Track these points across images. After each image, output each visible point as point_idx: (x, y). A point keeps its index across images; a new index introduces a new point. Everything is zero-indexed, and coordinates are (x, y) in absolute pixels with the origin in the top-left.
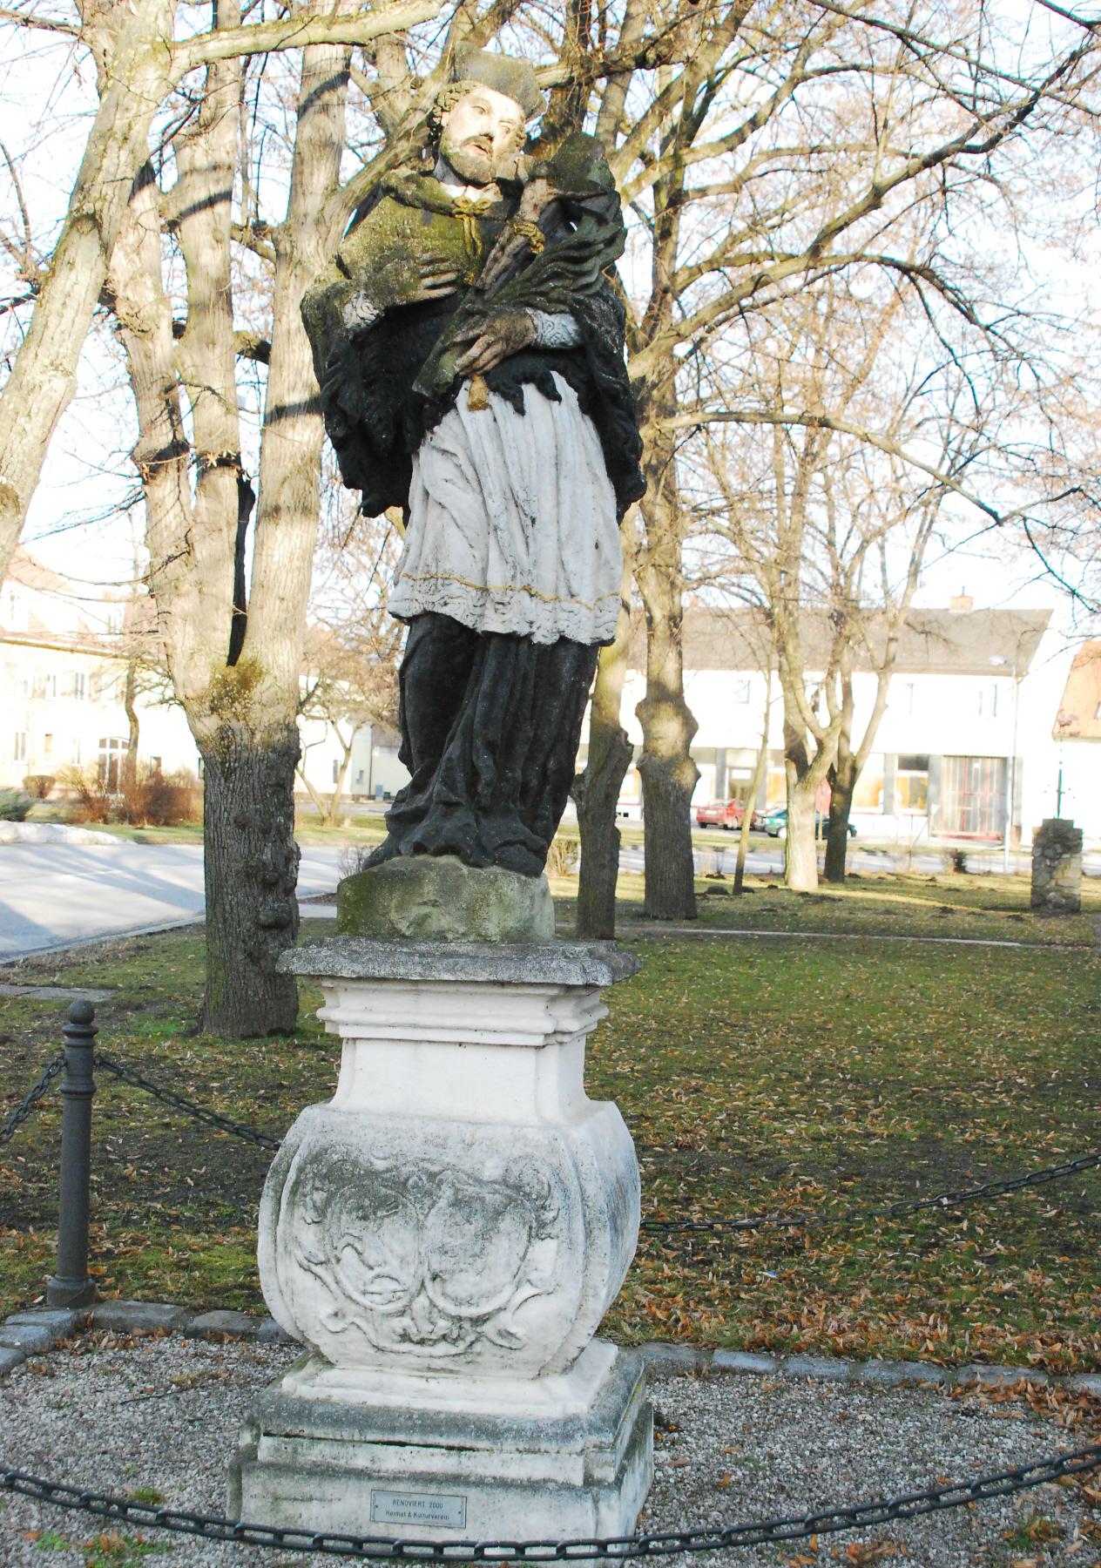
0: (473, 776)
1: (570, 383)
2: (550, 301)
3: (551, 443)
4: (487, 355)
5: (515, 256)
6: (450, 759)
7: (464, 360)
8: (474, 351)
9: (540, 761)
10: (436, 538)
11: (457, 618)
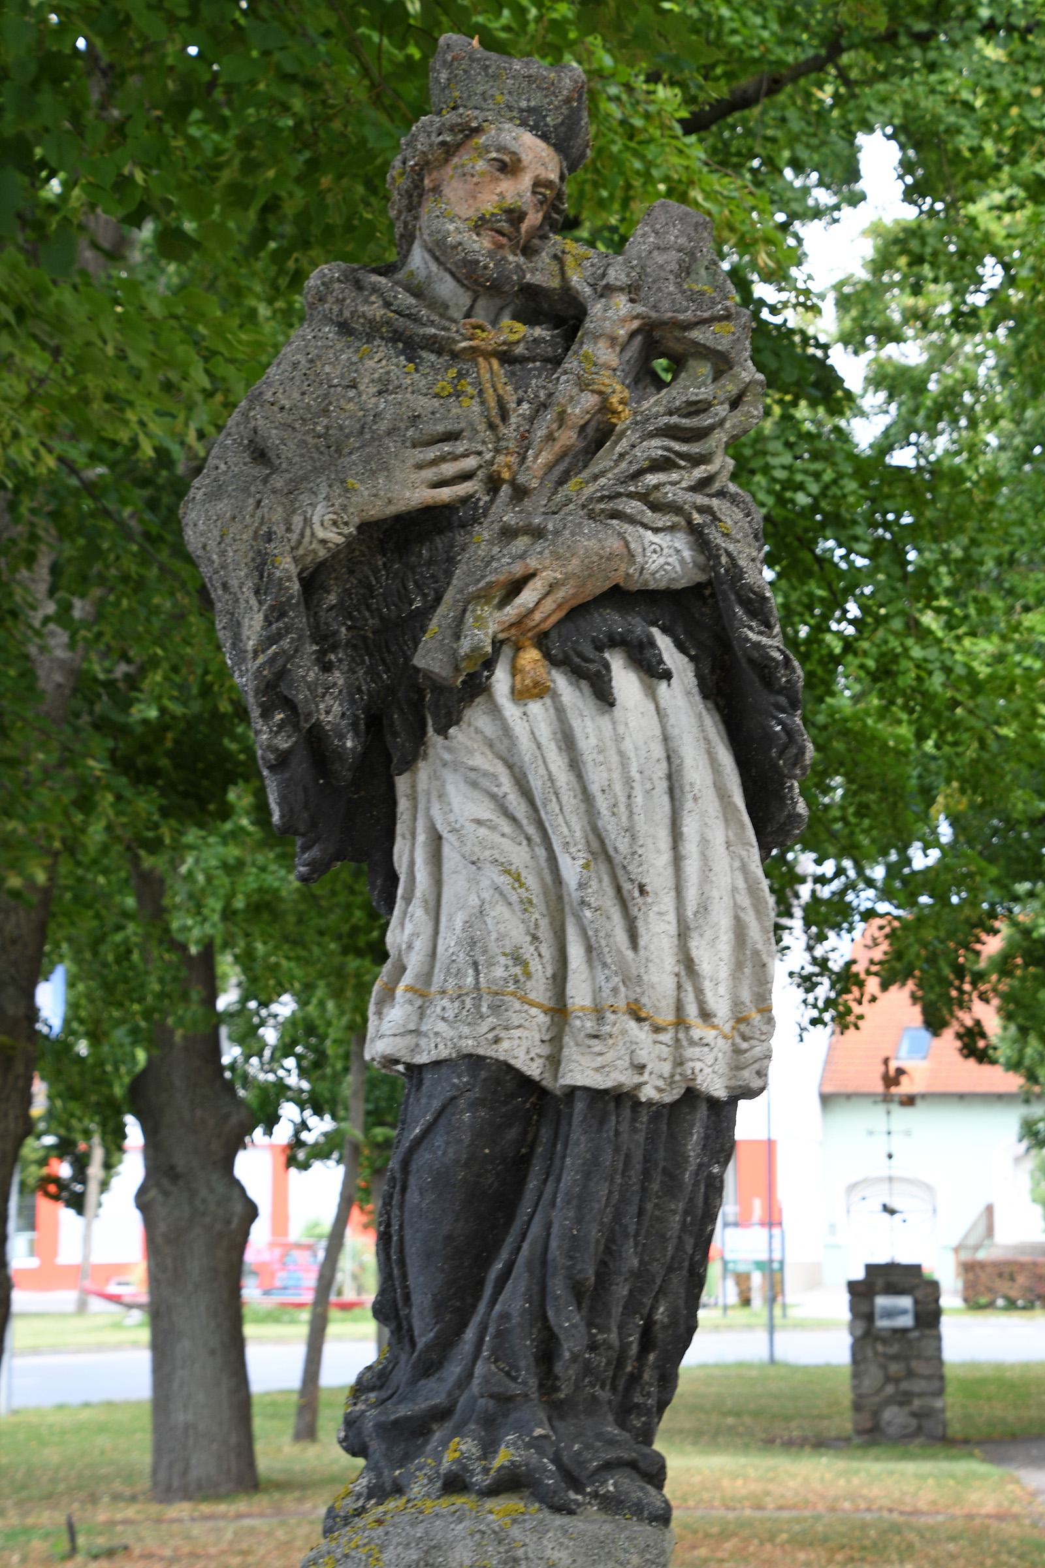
0: (547, 1353)
1: (681, 647)
2: (655, 507)
3: (658, 751)
4: (549, 605)
5: (583, 428)
6: (505, 1316)
7: (512, 611)
8: (528, 597)
9: (646, 1311)
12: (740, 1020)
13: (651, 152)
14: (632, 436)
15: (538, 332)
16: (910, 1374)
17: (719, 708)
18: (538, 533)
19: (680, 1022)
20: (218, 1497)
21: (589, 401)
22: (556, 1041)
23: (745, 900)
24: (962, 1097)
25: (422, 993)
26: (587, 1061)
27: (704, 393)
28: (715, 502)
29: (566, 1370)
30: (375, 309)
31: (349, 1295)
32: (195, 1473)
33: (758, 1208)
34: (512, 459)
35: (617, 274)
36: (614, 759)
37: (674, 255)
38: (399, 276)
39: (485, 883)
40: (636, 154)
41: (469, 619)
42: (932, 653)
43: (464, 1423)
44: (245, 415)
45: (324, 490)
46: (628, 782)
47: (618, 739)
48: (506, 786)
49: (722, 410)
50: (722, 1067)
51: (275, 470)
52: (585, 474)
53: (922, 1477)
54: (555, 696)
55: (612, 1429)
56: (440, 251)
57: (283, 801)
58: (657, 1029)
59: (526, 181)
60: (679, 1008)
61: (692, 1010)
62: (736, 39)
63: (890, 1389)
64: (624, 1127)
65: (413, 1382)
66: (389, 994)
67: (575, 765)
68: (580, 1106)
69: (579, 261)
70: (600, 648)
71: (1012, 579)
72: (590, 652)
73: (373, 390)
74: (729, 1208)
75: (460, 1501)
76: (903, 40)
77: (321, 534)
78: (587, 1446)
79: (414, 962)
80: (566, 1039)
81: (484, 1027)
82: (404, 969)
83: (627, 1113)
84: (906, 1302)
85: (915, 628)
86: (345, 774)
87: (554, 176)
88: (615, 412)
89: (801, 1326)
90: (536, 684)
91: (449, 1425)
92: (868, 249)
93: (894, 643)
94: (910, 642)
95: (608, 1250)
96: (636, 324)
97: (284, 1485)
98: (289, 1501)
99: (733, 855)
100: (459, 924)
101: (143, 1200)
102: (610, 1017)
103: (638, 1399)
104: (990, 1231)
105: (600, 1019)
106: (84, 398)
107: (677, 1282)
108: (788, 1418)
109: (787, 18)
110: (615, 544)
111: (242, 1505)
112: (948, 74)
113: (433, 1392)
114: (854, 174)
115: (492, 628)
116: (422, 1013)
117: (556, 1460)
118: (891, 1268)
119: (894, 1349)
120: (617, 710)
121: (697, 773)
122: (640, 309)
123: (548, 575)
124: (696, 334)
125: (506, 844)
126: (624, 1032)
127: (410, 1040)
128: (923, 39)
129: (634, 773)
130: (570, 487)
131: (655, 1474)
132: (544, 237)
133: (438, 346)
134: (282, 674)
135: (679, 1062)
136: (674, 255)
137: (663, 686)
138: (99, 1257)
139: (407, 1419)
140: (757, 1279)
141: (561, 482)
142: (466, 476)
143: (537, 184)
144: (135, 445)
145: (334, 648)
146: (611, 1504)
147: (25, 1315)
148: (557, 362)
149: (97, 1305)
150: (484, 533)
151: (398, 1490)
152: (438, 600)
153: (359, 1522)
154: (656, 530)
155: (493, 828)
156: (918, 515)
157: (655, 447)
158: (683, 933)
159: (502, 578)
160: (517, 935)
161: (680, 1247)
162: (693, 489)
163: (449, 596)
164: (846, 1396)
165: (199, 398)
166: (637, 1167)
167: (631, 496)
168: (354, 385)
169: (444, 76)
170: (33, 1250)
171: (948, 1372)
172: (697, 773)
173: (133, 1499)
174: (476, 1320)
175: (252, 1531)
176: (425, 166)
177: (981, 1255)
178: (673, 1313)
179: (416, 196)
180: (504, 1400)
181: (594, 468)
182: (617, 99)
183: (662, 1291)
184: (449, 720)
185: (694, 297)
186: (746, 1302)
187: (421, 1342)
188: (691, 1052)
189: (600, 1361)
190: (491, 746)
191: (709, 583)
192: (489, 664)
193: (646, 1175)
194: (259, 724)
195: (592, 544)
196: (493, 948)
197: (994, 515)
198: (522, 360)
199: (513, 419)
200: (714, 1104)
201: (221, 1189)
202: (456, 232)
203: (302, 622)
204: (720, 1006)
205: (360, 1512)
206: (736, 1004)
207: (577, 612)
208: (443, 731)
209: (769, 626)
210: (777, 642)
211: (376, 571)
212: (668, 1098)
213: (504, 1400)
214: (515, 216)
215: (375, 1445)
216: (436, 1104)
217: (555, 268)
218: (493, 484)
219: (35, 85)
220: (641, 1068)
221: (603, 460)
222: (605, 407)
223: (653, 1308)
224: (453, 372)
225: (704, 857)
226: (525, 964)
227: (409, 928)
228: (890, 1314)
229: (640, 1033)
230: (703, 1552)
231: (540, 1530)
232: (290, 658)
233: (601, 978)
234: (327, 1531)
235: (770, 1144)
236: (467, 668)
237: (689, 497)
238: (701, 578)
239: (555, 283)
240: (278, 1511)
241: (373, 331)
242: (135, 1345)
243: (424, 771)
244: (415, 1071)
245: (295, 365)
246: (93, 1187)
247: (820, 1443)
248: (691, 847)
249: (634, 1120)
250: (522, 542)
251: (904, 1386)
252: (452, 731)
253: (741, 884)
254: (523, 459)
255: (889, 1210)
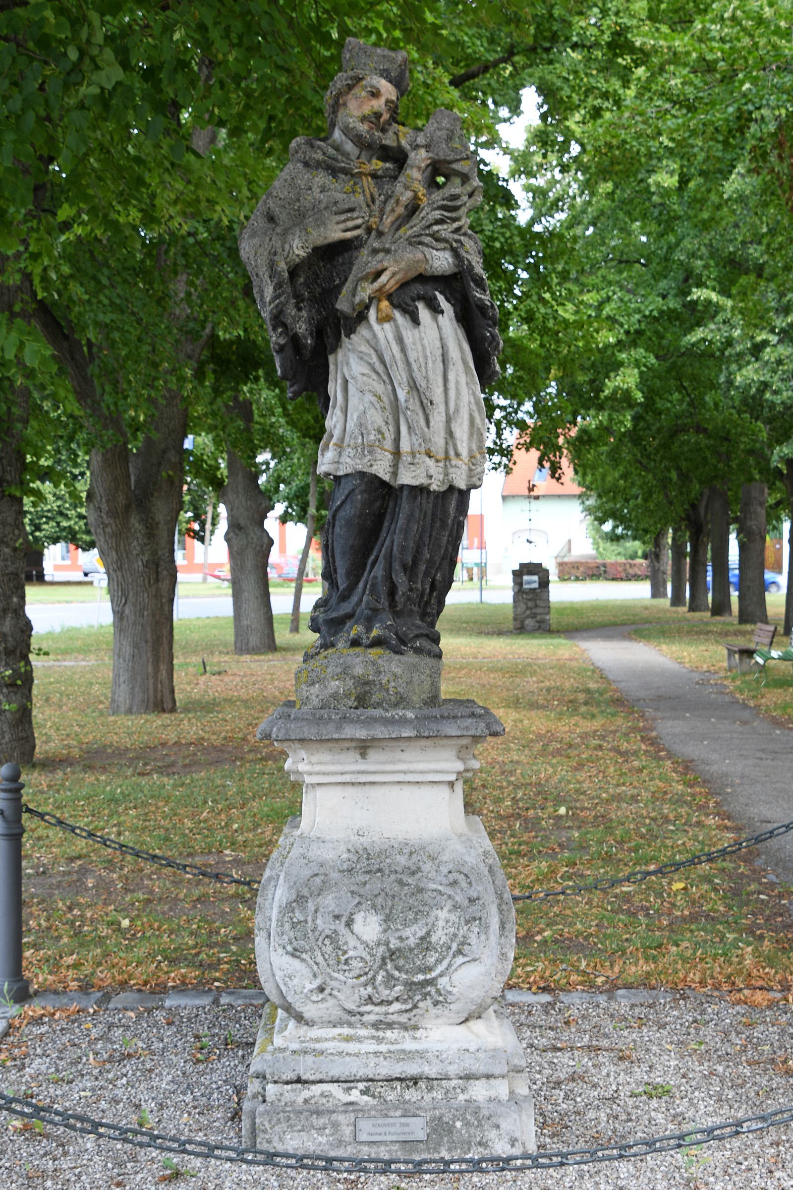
0: (392, 592)
2: (437, 240)
4: (392, 282)
5: (406, 206)
6: (375, 578)
7: (376, 285)
8: (384, 278)
10: (359, 417)
11: (380, 475)
12: (472, 457)
13: (435, 94)
14: (427, 209)
15: (388, 165)
16: (536, 606)
17: (464, 326)
18: (387, 251)
19: (447, 458)
20: (262, 654)
21: (409, 194)
22: (395, 466)
23: (474, 407)
24: (559, 496)
25: (340, 446)
26: (408, 474)
27: (457, 191)
28: (462, 238)
29: (400, 598)
30: (319, 156)
31: (311, 577)
32: (251, 644)
33: (476, 542)
34: (377, 220)
35: (421, 140)
36: (420, 348)
37: (445, 132)
38: (330, 141)
39: (366, 400)
40: (430, 95)
41: (359, 288)
42: (549, 311)
43: (359, 619)
44: (265, 202)
45: (298, 233)
46: (426, 357)
47: (421, 339)
48: (375, 359)
49: (465, 198)
50: (464, 476)
51: (277, 225)
52: (407, 226)
53: (540, 645)
54: (395, 320)
55: (419, 622)
56: (346, 131)
57: (282, 366)
58: (437, 461)
59: (382, 100)
60: (447, 452)
61: (452, 453)
62: (469, 51)
63: (528, 612)
64: (424, 502)
65: (338, 603)
66: (327, 447)
67: (403, 350)
68: (405, 493)
69: (405, 135)
70: (414, 301)
71: (583, 279)
72: (409, 302)
73: (318, 190)
74: (465, 542)
75: (358, 650)
76: (539, 50)
77: (297, 252)
78: (409, 629)
79: (337, 433)
80: (400, 465)
81: (366, 460)
82: (332, 436)
83: (425, 495)
84: (536, 578)
85: (542, 300)
86: (307, 354)
87: (394, 98)
88: (420, 199)
89: (493, 588)
90: (387, 316)
91: (352, 621)
92: (525, 136)
93: (533, 305)
94: (540, 306)
95: (417, 551)
96: (429, 162)
97: (286, 649)
98: (289, 655)
99: (469, 388)
100: (355, 417)
101: (227, 538)
102: (418, 456)
103: (429, 610)
104: (570, 550)
105: (414, 457)
106: (198, 201)
107: (446, 565)
108: (487, 624)
109: (492, 41)
110: (420, 256)
111: (270, 657)
112: (557, 65)
113: (346, 608)
114: (518, 107)
115: (369, 292)
116: (340, 454)
117: (396, 634)
118: (530, 565)
119: (531, 596)
120: (421, 327)
121: (454, 353)
122: (431, 155)
123: (392, 269)
124: (455, 166)
125: (375, 383)
126: (424, 462)
127: (336, 466)
128: (548, 50)
129: (428, 354)
130: (401, 231)
131: (436, 640)
132: (390, 125)
133: (346, 172)
134: (281, 312)
135: (447, 474)
136: (445, 132)
137: (440, 316)
138: (211, 560)
139: (336, 618)
140: (475, 570)
141: (398, 229)
142: (357, 227)
143: (388, 101)
144: (221, 220)
145: (302, 301)
146: (418, 651)
147: (183, 583)
148: (395, 178)
149: (210, 579)
150: (365, 251)
151: (333, 645)
152: (346, 280)
153: (317, 658)
154: (437, 250)
155: (369, 377)
156: (545, 252)
157: (437, 214)
158: (449, 421)
159: (373, 270)
160: (380, 422)
161: (446, 550)
162: (453, 232)
163: (351, 278)
164: (511, 615)
165: (246, 201)
166: (429, 517)
167: (427, 235)
168: (310, 188)
169: (348, 56)
170: (184, 558)
171: (551, 605)
172: (454, 353)
173: (228, 653)
174: (363, 579)
175: (274, 666)
176: (340, 94)
177: (566, 560)
178: (443, 576)
179: (336, 106)
180: (375, 611)
181: (411, 223)
182: (422, 72)
183: (439, 568)
184: (351, 331)
185: (454, 150)
186: (471, 579)
187: (341, 588)
188: (451, 470)
189: (414, 595)
190: (368, 342)
191: (460, 273)
192: (367, 307)
193: (433, 521)
194: (272, 333)
195: (411, 256)
196: (370, 427)
197: (575, 253)
198: (381, 177)
199: (377, 203)
200: (460, 491)
201: (259, 534)
202: (353, 122)
203: (289, 290)
204: (464, 452)
205: (317, 654)
206: (470, 450)
207: (404, 285)
208: (348, 336)
209: (485, 291)
210: (488, 298)
211: (320, 268)
212: (442, 489)
213: (375, 611)
214: (378, 115)
215: (323, 628)
216: (346, 492)
217: (395, 137)
218: (369, 230)
219: (175, 70)
220: (431, 477)
221: (415, 220)
222: (416, 197)
223: (436, 575)
224: (352, 183)
225: (457, 389)
226: (383, 434)
227: (334, 419)
228: (529, 583)
229: (430, 463)
230: (453, 674)
231: (390, 661)
232: (284, 305)
233: (414, 439)
234: (305, 661)
235: (482, 516)
236: (358, 309)
237: (451, 235)
238: (456, 270)
239: (395, 144)
240: (284, 659)
241: (318, 165)
242: (226, 595)
243: (340, 354)
244: (337, 479)
245: (286, 180)
246: (208, 533)
247: (500, 633)
248: (452, 385)
249: (428, 498)
250: (381, 255)
251: (534, 611)
252: (352, 336)
253: (472, 400)
254: (381, 219)
255: (529, 542)
